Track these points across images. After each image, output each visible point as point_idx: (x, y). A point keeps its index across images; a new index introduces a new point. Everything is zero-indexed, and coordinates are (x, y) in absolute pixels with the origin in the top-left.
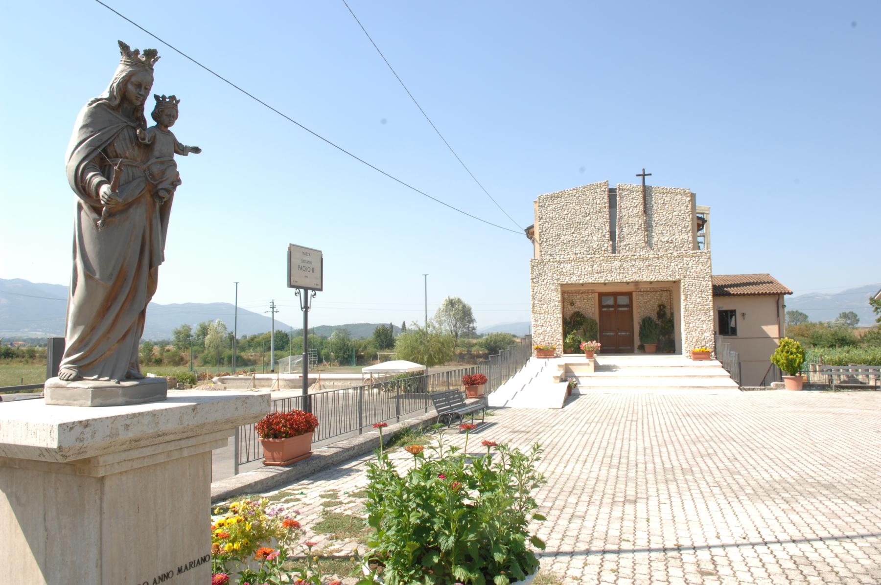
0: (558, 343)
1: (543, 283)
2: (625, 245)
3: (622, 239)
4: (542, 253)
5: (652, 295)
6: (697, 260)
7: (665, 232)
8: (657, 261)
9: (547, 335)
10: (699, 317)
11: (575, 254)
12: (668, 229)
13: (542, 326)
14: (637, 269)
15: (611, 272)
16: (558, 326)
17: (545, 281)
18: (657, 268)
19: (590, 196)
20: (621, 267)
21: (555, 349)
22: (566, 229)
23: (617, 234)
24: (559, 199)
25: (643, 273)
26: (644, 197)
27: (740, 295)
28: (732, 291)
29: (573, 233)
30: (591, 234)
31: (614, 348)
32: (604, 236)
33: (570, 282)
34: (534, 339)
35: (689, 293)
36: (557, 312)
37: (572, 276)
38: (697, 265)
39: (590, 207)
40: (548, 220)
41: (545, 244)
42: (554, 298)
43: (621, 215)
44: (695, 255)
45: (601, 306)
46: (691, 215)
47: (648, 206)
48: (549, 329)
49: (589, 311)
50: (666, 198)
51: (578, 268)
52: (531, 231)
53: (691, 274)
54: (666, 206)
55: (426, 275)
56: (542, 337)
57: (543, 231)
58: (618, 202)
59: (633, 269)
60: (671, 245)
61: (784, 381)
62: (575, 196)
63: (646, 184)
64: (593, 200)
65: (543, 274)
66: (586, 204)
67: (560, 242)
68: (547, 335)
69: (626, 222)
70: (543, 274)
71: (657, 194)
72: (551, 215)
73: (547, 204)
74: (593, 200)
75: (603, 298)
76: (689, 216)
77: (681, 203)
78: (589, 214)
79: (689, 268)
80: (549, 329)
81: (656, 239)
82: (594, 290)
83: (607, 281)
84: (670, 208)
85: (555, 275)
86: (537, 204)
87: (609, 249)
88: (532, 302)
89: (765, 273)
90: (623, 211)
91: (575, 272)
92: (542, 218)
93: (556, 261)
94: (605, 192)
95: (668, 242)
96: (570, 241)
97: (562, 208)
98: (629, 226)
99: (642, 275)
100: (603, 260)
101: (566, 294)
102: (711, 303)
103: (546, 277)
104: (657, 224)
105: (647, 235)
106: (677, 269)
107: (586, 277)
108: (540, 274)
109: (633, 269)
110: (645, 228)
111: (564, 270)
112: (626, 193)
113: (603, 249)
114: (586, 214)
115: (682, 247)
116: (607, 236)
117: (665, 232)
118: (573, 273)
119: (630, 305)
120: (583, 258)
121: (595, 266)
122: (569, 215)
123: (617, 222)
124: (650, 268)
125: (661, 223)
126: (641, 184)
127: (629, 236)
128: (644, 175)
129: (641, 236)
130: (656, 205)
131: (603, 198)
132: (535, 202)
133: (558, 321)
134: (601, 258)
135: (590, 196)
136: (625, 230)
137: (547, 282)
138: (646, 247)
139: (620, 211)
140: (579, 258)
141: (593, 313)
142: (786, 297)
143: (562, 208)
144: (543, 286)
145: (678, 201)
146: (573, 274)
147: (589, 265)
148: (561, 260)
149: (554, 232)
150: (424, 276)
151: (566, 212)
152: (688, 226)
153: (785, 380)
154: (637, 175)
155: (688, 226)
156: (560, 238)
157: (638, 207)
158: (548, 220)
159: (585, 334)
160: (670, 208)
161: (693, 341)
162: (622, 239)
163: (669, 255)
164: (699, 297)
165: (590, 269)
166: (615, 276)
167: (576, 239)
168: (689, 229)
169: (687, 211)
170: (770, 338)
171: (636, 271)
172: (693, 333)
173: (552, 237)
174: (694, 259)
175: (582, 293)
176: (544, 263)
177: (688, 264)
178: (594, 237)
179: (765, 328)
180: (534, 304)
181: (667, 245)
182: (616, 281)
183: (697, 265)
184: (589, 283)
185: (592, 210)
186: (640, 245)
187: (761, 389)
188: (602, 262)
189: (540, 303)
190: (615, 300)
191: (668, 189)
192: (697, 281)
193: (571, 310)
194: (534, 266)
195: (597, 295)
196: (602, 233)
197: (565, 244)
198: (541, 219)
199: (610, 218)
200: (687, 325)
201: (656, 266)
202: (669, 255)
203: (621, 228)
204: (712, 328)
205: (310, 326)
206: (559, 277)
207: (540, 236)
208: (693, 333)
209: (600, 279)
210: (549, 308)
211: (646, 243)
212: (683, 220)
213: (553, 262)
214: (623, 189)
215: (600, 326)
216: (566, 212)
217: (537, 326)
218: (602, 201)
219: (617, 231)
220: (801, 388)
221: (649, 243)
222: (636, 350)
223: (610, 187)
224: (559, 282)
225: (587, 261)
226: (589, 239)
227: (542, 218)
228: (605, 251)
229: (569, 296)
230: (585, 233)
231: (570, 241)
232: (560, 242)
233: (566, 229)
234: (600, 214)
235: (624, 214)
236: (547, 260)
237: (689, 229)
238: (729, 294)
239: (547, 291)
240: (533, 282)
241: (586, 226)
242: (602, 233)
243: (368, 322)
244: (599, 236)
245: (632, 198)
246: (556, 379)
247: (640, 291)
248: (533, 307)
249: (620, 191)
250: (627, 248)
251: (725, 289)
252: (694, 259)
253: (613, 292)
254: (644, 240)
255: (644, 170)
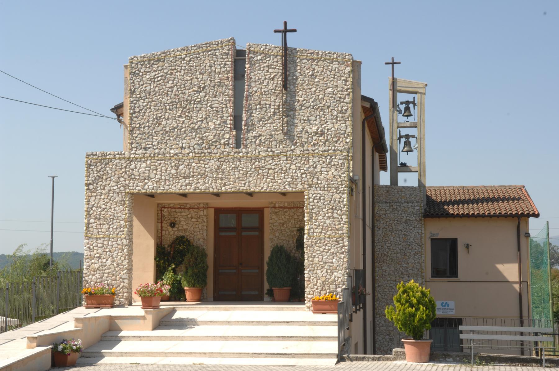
0: (122, 284)
1: (104, 192)
2: (255, 137)
3: (251, 127)
4: (133, 146)
5: (292, 214)
6: (328, 161)
7: (313, 118)
8: (270, 162)
9: (107, 271)
10: (327, 248)
11: (182, 148)
12: (318, 113)
13: (99, 257)
14: (241, 172)
15: (204, 176)
16: (123, 258)
17: (107, 188)
18: (271, 171)
19: (207, 61)
20: (218, 168)
21: (114, 294)
22: (170, 109)
23: (244, 119)
24: (161, 64)
25: (251, 179)
26: (285, 66)
27: (463, 216)
28: (451, 209)
29: (180, 116)
30: (206, 118)
31: (234, 293)
32: (225, 122)
33: (144, 191)
34: (87, 278)
35: (314, 211)
36: (123, 236)
37: (146, 181)
38: (328, 169)
39: (205, 78)
40: (143, 95)
41: (138, 132)
42: (119, 215)
43: (250, 91)
44: (326, 153)
45: (218, 229)
46: (351, 94)
47: (290, 78)
48: (109, 262)
49: (199, 236)
50: (316, 68)
51: (156, 170)
52: (120, 111)
53: (319, 182)
54: (316, 80)
55: (53, 178)
56: (98, 275)
57: (135, 113)
58: (247, 71)
59: (236, 173)
60: (320, 138)
61: (404, 348)
62: (184, 59)
63: (289, 45)
64: (211, 66)
65: (104, 177)
66: (200, 73)
67: (159, 129)
68: (107, 271)
69: (257, 102)
70: (104, 177)
71: (304, 61)
72: (148, 88)
73: (142, 70)
74: (211, 66)
75: (222, 216)
76: (348, 95)
77: (338, 74)
78: (204, 88)
79: (317, 172)
80: (109, 262)
81: (299, 129)
82: (207, 204)
83: (198, 191)
84: (321, 82)
85: (122, 179)
86: (128, 71)
87: (231, 141)
88: (86, 221)
89: (518, 183)
90: (253, 84)
91: (152, 176)
92: (134, 91)
93: (124, 158)
94: (227, 54)
95: (316, 133)
96: (175, 128)
97: (164, 77)
98: (261, 108)
99: (249, 182)
100: (193, 158)
101: (166, 210)
102: (346, 227)
103: (108, 182)
104: (302, 105)
105: (287, 123)
106: (299, 175)
107: (168, 183)
108: (99, 177)
109: (236, 173)
110: (283, 111)
111: (135, 173)
112: (259, 57)
113: (222, 141)
114: (199, 87)
115: (336, 142)
116: (229, 122)
117: (313, 118)
118: (149, 176)
119: (261, 228)
120: (164, 154)
121: (181, 167)
122: (175, 89)
123: (244, 102)
124: (260, 171)
125: (308, 105)
126: (279, 44)
127: (261, 122)
128: (285, 31)
129: (277, 124)
130: (301, 78)
131: (225, 64)
132: (126, 67)
133: (123, 250)
134: (191, 154)
135: (207, 61)
136: (256, 114)
137: (110, 190)
138: (285, 140)
139: (250, 86)
140: (159, 154)
141: (204, 239)
142: (531, 220)
143: (165, 79)
144: (102, 197)
145: (333, 73)
146: (149, 178)
147: (173, 165)
148: (132, 156)
149: (152, 114)
150: (51, 179)
151: (170, 84)
152: (346, 110)
153: (406, 345)
154: (295, 31)
155: (346, 110)
156: (160, 124)
157: (276, 79)
158: (143, 95)
159: (187, 272)
160: (321, 82)
161: (318, 284)
162: (250, 128)
163: (289, 153)
164: (329, 218)
165: (173, 171)
166: (210, 182)
167: (184, 126)
168: (347, 115)
169: (346, 87)
170: (509, 282)
171: (241, 175)
172: (319, 272)
173: (148, 121)
174: (324, 160)
175: (190, 208)
176: (106, 161)
177: (315, 168)
178: (210, 123)
179: (500, 267)
180: (89, 223)
181: (315, 138)
182: (211, 190)
183: (328, 169)
184: (171, 193)
185: (209, 82)
186: (276, 137)
187: (374, 359)
188: (191, 161)
189: (98, 223)
190: (239, 219)
191: (320, 53)
192: (326, 193)
193: (171, 234)
194: (90, 165)
195: (212, 211)
196: (222, 117)
197: (167, 132)
198: (132, 92)
199: (235, 96)
200: (310, 259)
201: (269, 169)
202: (289, 153)
203: (249, 110)
204: (345, 265)
205: (54, 251)
206: (127, 182)
207: (131, 119)
208: (319, 272)
209: (188, 187)
210: (111, 229)
211: (285, 134)
212: (339, 101)
213: (120, 159)
214: (254, 52)
215: (215, 259)
216: (170, 84)
217: (91, 257)
218: (223, 69)
219: (244, 115)
220: (427, 358)
221: (289, 135)
222: (266, 298)
223: (238, 48)
224: (127, 190)
225: (170, 159)
226: (203, 125)
227: (134, 91)
228: (225, 145)
229: (170, 214)
230: (197, 117)
231: (175, 128)
232: (159, 129)
233: (170, 109)
234: (220, 89)
235: (255, 89)
236: (112, 157)
237: (347, 115)
238: (447, 215)
239: (109, 204)
240: (88, 189)
241: (199, 106)
242: (222, 117)
243: (75, 250)
244: (218, 122)
245: (268, 66)
246: (31, 342)
247: (275, 208)
248: (88, 228)
249: (251, 55)
250: (258, 142)
251: (446, 207)
252: (324, 160)
253: (235, 208)
254: (282, 130)
255: (285, 23)
